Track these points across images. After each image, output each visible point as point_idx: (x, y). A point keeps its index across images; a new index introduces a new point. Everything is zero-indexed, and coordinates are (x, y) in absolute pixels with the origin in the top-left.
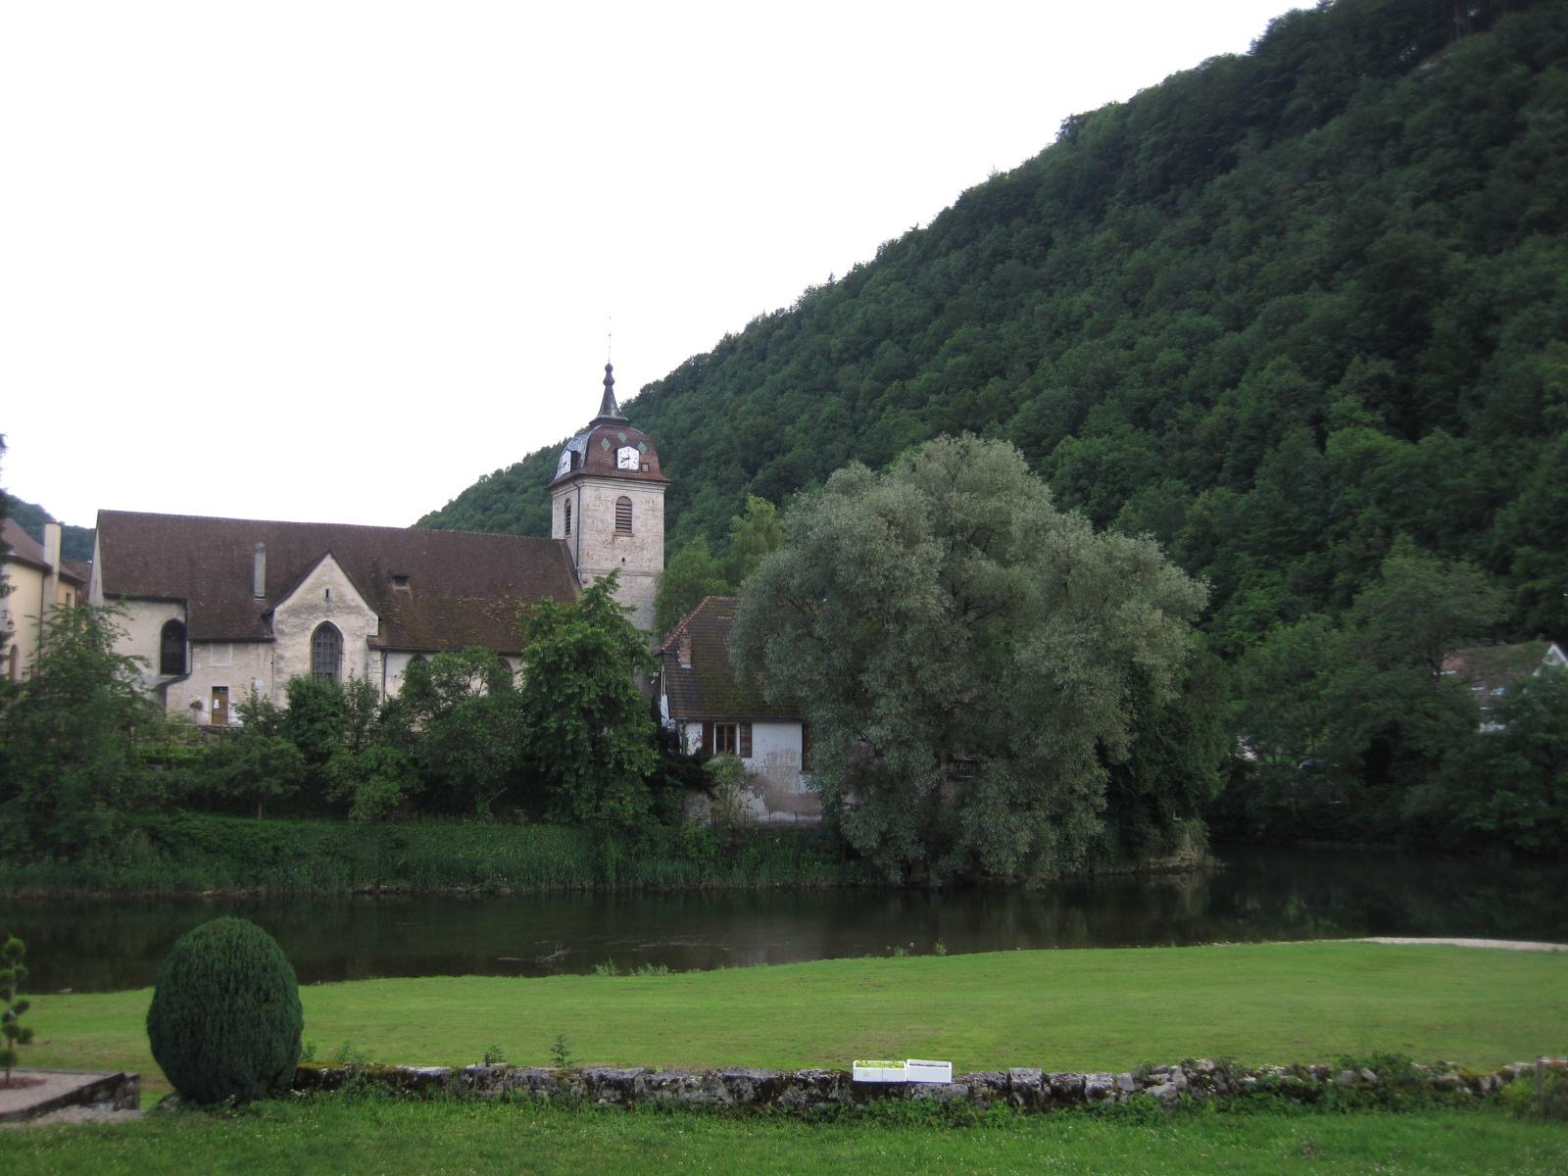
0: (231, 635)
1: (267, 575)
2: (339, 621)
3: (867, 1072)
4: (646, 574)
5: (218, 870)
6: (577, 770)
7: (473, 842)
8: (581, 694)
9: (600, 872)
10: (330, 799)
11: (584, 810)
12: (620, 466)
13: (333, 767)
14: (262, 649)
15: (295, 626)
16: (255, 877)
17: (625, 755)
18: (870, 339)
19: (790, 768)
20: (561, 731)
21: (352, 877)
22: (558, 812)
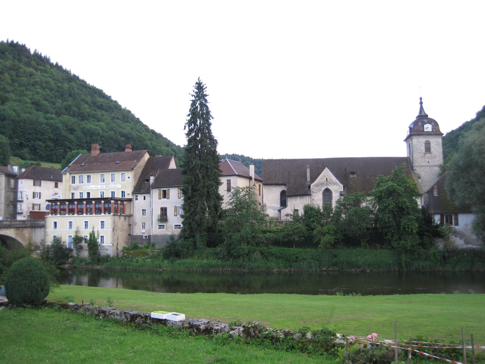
0: (298, 194)
2: (331, 188)
3: (155, 315)
4: (436, 166)
8: (389, 206)
10: (314, 242)
11: (395, 244)
12: (425, 130)
13: (315, 232)
14: (307, 197)
15: (317, 190)
16: (290, 266)
21: (319, 266)
22: (387, 245)
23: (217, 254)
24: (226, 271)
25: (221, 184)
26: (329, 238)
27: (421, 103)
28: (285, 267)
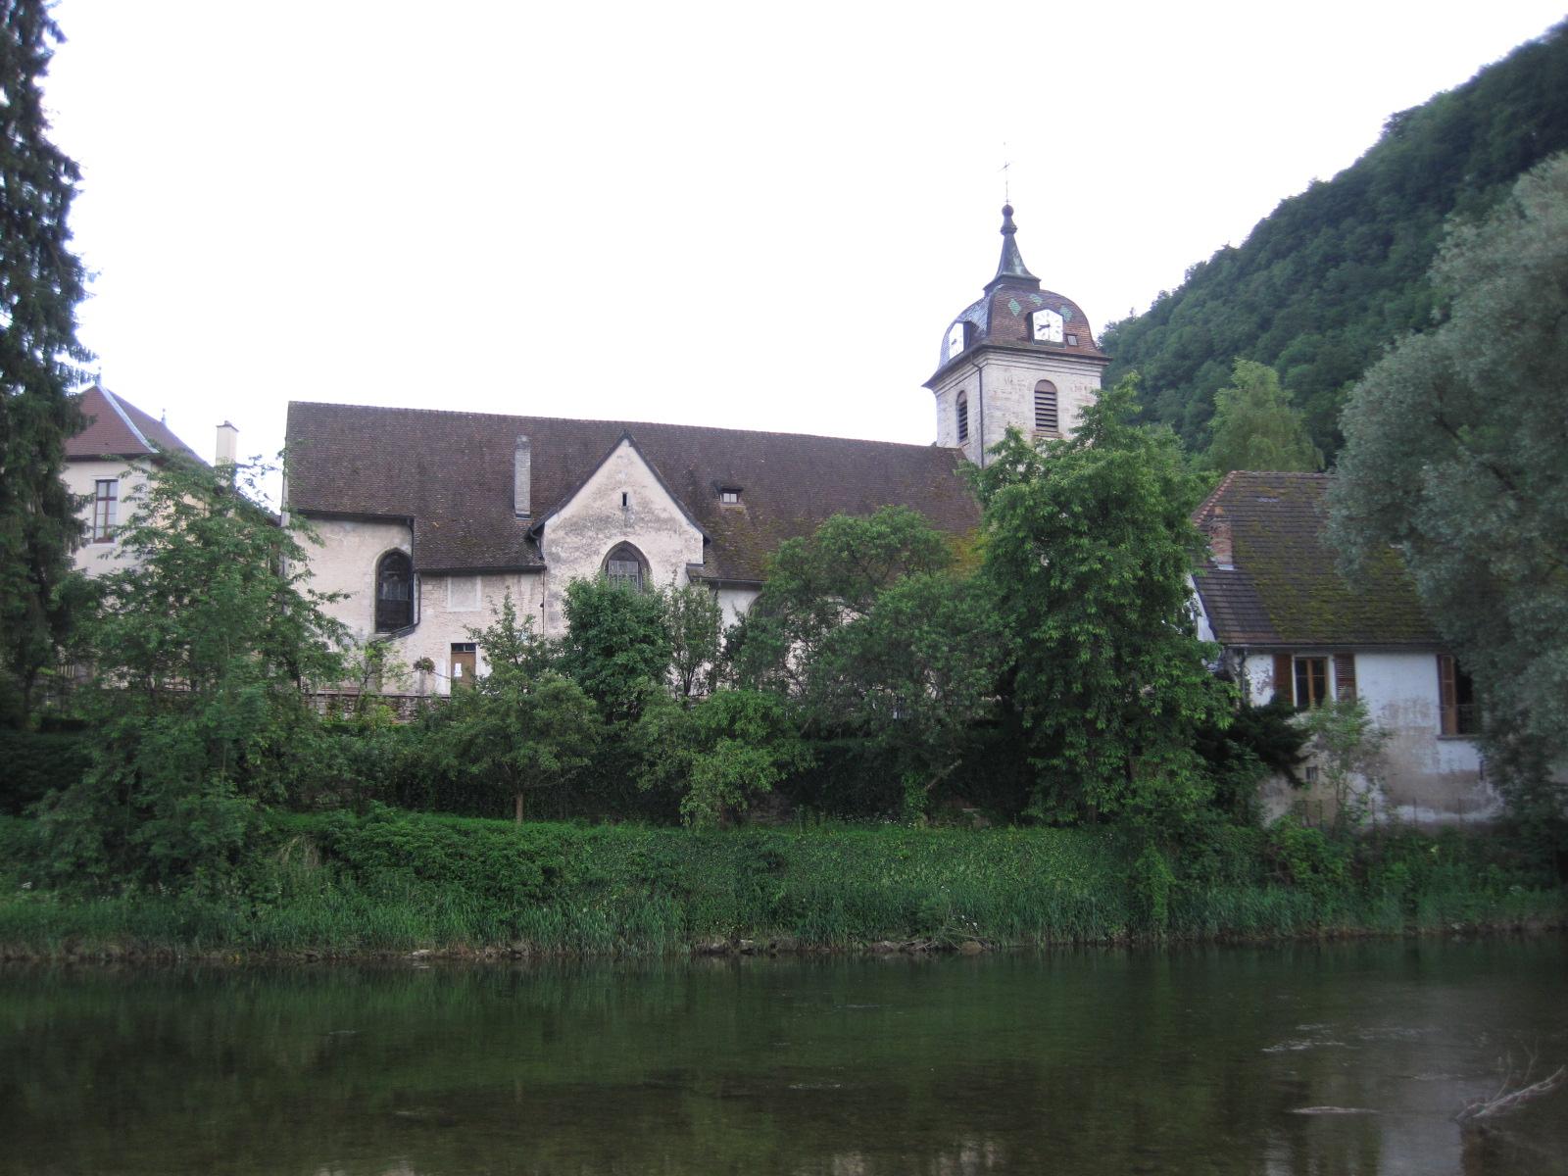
0: (479, 563)
1: (533, 485)
2: (642, 542)
5: (441, 911)
6: (1093, 722)
7: (906, 858)
9: (1139, 910)
10: (644, 784)
12: (1038, 336)
15: (577, 549)
17: (1180, 692)
18: (1188, 363)
19: (1422, 730)
20: (1068, 645)
21: (689, 926)
22: (1051, 803)
23: (32, 852)
24: (93, 959)
25: (83, 428)
26: (743, 758)
27: (1009, 230)
28: (480, 931)
